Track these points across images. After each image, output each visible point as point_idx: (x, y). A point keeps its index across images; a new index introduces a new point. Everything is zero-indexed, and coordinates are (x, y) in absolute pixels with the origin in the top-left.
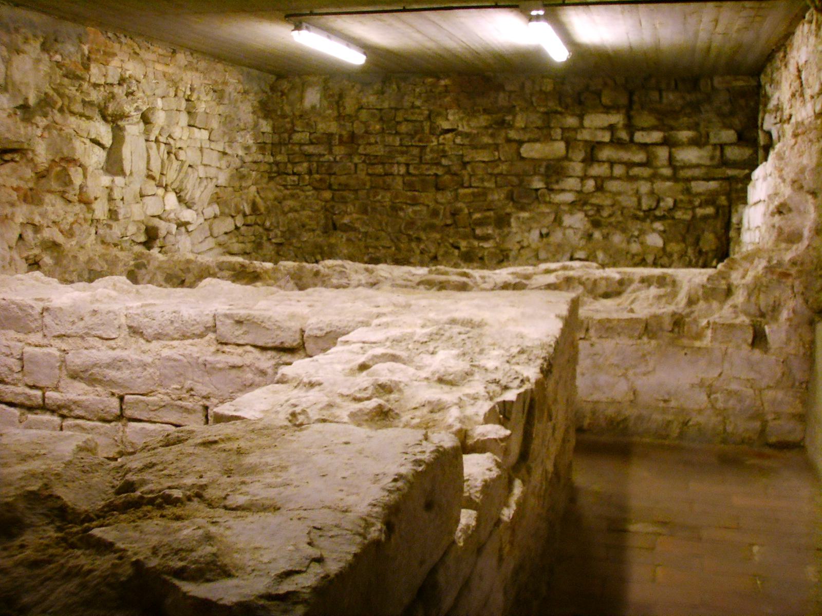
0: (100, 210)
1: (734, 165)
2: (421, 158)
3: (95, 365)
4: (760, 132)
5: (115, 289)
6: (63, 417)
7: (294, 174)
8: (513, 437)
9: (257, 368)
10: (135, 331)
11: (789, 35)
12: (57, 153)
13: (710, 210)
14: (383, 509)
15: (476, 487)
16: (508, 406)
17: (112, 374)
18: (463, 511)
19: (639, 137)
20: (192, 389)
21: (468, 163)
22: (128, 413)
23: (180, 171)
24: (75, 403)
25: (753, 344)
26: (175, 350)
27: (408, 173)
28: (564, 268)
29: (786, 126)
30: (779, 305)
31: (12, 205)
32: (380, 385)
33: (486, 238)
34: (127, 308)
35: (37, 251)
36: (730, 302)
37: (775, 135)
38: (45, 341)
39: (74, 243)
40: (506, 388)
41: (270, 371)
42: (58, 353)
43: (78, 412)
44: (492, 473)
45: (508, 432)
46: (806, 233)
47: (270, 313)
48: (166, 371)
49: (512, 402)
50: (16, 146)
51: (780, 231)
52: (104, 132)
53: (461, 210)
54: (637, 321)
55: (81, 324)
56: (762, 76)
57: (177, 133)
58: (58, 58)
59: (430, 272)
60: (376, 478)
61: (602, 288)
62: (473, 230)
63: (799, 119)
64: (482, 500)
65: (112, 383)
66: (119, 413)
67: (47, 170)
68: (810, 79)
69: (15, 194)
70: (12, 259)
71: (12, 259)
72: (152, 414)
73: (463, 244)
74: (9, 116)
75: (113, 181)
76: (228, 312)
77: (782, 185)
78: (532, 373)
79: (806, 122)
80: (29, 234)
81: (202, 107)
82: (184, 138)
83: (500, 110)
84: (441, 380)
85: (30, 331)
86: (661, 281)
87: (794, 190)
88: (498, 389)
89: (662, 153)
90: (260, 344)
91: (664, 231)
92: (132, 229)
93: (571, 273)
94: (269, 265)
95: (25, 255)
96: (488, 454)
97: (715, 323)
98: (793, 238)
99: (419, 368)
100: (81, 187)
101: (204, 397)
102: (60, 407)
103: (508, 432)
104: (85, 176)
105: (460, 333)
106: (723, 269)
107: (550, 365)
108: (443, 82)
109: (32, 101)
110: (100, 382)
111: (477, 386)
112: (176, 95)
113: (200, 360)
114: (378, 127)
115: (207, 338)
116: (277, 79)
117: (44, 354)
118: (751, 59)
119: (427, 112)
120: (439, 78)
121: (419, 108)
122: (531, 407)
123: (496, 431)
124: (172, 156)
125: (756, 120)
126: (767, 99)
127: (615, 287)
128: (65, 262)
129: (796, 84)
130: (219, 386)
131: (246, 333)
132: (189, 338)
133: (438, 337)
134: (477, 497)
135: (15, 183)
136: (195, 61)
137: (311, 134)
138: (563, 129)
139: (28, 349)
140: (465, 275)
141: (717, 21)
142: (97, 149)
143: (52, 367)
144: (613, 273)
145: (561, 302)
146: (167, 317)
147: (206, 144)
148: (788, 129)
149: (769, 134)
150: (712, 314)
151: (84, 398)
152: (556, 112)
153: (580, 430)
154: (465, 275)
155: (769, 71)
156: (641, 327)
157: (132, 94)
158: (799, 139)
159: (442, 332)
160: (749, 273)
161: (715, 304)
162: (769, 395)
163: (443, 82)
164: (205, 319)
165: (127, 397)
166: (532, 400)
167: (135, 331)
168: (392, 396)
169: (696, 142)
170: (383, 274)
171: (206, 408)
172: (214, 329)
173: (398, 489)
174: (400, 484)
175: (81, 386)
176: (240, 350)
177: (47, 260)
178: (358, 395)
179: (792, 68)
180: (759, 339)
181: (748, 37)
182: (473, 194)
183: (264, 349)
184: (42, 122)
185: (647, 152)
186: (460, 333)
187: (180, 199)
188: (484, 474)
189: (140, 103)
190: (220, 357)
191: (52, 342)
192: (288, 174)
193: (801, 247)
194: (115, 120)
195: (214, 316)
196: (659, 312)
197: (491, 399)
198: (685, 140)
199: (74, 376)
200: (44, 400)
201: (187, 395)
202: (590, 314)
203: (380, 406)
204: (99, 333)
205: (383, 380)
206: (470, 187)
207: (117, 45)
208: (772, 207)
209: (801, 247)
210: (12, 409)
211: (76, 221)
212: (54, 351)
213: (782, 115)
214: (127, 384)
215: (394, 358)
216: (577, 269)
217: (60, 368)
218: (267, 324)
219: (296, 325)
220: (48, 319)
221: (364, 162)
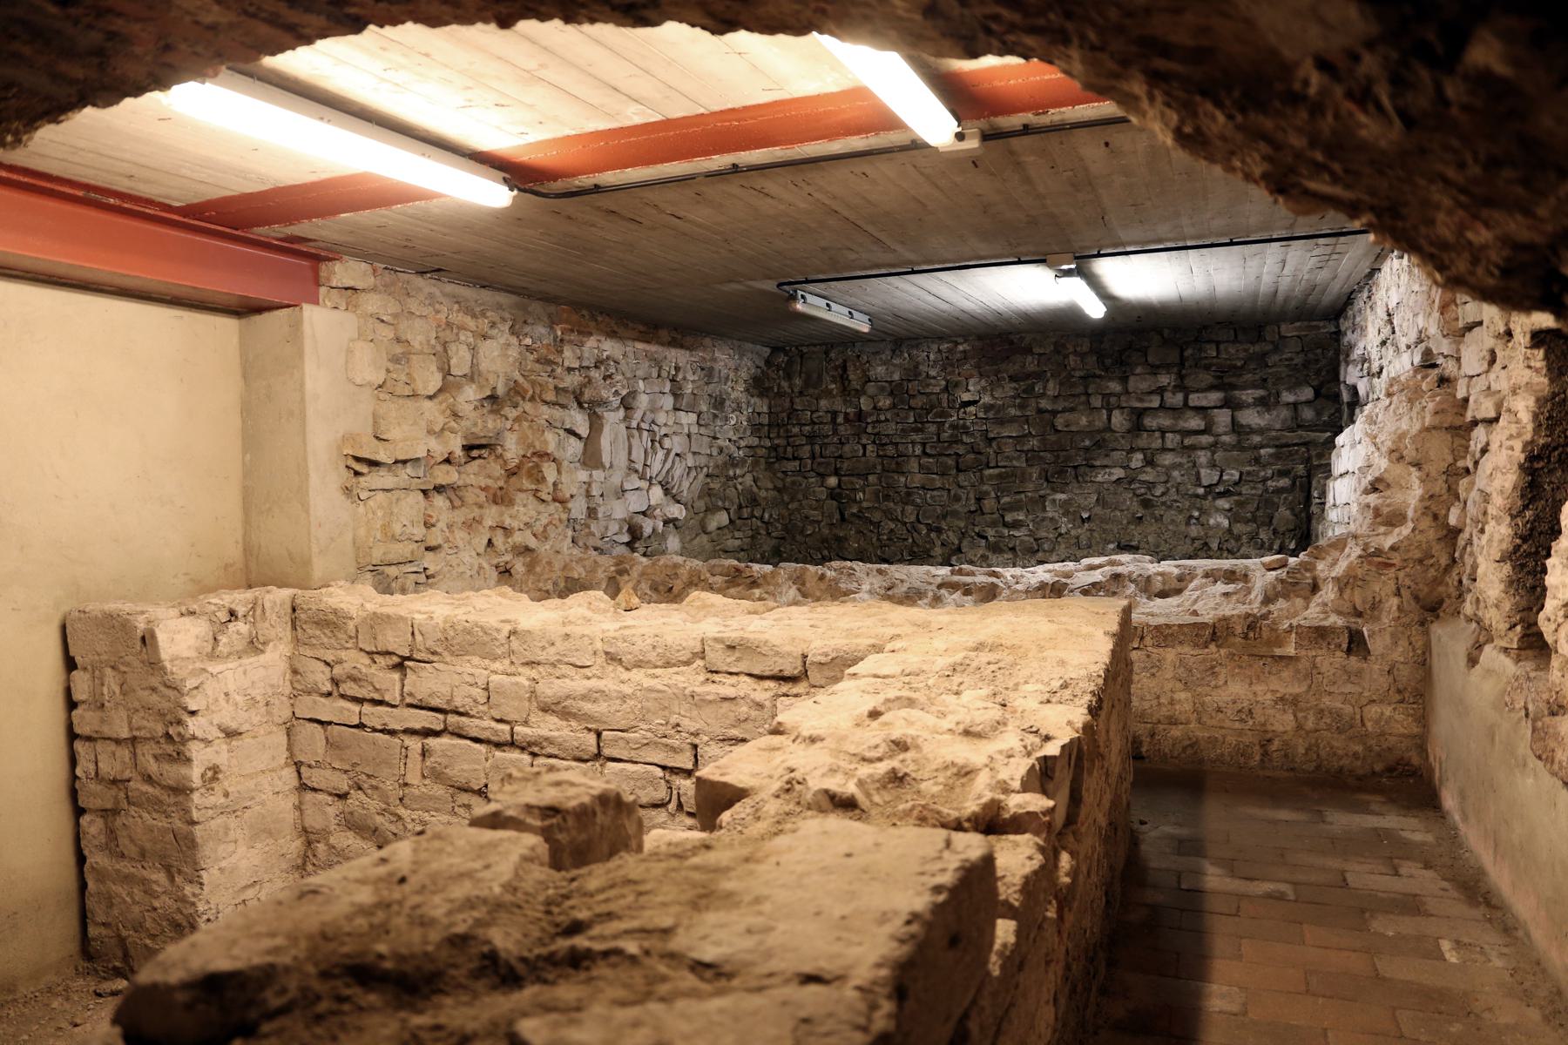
0: (578, 508)
1: (1311, 427)
2: (938, 435)
3: (568, 697)
4: (1342, 386)
5: (589, 608)
6: (534, 755)
7: (795, 458)
8: (1057, 810)
9: (752, 701)
10: (612, 658)
11: (1374, 271)
12: (529, 447)
13: (1284, 482)
14: (893, 969)
15: (1014, 885)
16: (1049, 763)
17: (588, 707)
18: (1000, 922)
19: (1195, 400)
20: (678, 725)
21: (994, 438)
22: (607, 752)
23: (665, 461)
24: (546, 739)
25: (1349, 651)
26: (656, 681)
27: (925, 453)
28: (1112, 563)
29: (1376, 380)
30: (1380, 601)
31: (481, 507)
32: (893, 742)
33: (1016, 525)
34: (603, 631)
35: (508, 558)
36: (1317, 599)
37: (1362, 391)
38: (512, 669)
39: (548, 547)
40: (1047, 738)
41: (767, 704)
42: (527, 683)
43: (550, 750)
44: (1034, 862)
45: (1051, 803)
46: (1410, 513)
47: (767, 636)
48: (649, 704)
49: (1054, 757)
50: (484, 442)
51: (1377, 512)
52: (580, 422)
53: (987, 493)
54: (1204, 625)
55: (552, 650)
56: (1341, 320)
57: (661, 418)
58: (528, 341)
59: (953, 573)
60: (884, 918)
61: (1158, 585)
62: (1003, 517)
63: (1392, 375)
64: (1022, 903)
65: (588, 717)
66: (596, 751)
67: (518, 467)
68: (1405, 324)
69: (482, 495)
70: (481, 567)
71: (481, 567)
72: (633, 753)
73: (990, 532)
74: (476, 408)
75: (591, 475)
76: (720, 635)
77: (1376, 454)
78: (1078, 714)
79: (1402, 378)
80: (499, 540)
81: (689, 388)
82: (670, 423)
83: (1028, 376)
84: (967, 733)
85: (495, 658)
86: (1230, 576)
87: (1391, 461)
88: (1037, 740)
89: (1223, 418)
90: (756, 672)
91: (1230, 510)
92: (614, 527)
93: (1119, 569)
94: (768, 568)
95: (495, 562)
96: (1027, 836)
97: (1299, 626)
98: (1393, 519)
99: (943, 715)
100: (555, 484)
101: (692, 734)
102: (530, 744)
103: (1051, 803)
104: (559, 472)
105: (989, 663)
106: (1307, 559)
107: (1100, 700)
108: (961, 348)
109: (500, 391)
110: (574, 716)
111: (1011, 739)
112: (659, 376)
113: (687, 692)
114: (888, 402)
115: (695, 665)
116: (772, 353)
117: (512, 684)
118: (1327, 299)
119: (944, 383)
120: (957, 344)
121: (934, 378)
122: (1079, 758)
123: (1037, 802)
124: (657, 444)
125: (1337, 374)
126: (1351, 347)
127: (1175, 585)
128: (538, 569)
129: (1386, 331)
130: (709, 721)
131: (738, 660)
132: (674, 665)
133: (963, 668)
134: (1015, 900)
135: (483, 482)
136: (679, 337)
137: (812, 412)
138: (1104, 396)
139: (494, 678)
140: (995, 574)
141: (1284, 262)
142: (572, 440)
143: (521, 699)
144: (1169, 567)
145: (1108, 612)
146: (649, 641)
147: (694, 429)
148: (1381, 384)
149: (1354, 390)
150: (1296, 614)
151: (556, 734)
152: (1095, 376)
153: (1138, 757)
154: (995, 574)
155: (1350, 313)
156: (1208, 632)
157: (610, 376)
158: (1395, 398)
159: (968, 662)
160: (1340, 563)
161: (1299, 602)
162: (1373, 711)
163: (961, 348)
164: (691, 643)
165: (605, 733)
166: (1080, 750)
167: (612, 658)
168: (909, 755)
169: (1263, 403)
170: (897, 575)
171: (695, 747)
172: (702, 655)
173: (913, 936)
174: (915, 928)
175: (553, 720)
176: (734, 679)
177: (519, 567)
178: (868, 755)
179: (1381, 312)
180: (1356, 643)
181: (1323, 276)
182: (1000, 476)
183: (761, 678)
184: (512, 413)
185: (1204, 418)
186: (989, 663)
187: (667, 492)
188: (1023, 865)
189: (619, 387)
190: (711, 688)
191: (521, 669)
192: (788, 459)
193: (1406, 530)
194: (593, 409)
195: (702, 640)
196: (1228, 613)
197: (1029, 754)
198: (1250, 400)
199: (545, 709)
200: (512, 736)
201: (672, 732)
202: (1144, 618)
203: (894, 771)
204: (572, 660)
205: (896, 734)
206: (997, 467)
207: (592, 324)
208: (1365, 482)
209: (1406, 530)
210: (477, 746)
211: (550, 523)
212: (522, 680)
213: (1369, 368)
214: (604, 719)
215: (911, 703)
216: (1128, 563)
217: (530, 699)
218: (764, 650)
219: (798, 651)
220: (515, 644)
221: (874, 442)
